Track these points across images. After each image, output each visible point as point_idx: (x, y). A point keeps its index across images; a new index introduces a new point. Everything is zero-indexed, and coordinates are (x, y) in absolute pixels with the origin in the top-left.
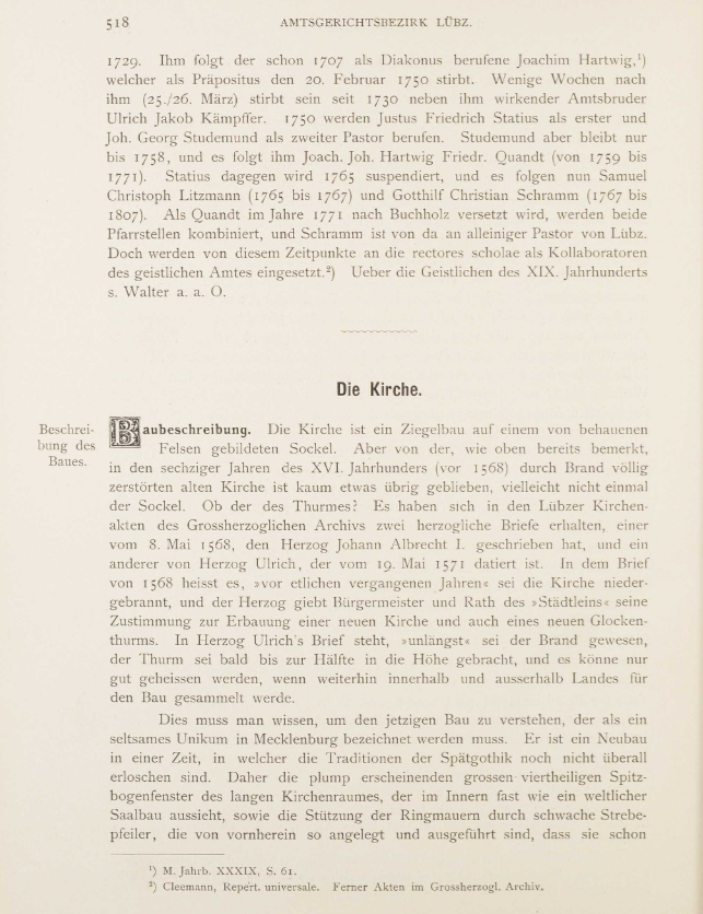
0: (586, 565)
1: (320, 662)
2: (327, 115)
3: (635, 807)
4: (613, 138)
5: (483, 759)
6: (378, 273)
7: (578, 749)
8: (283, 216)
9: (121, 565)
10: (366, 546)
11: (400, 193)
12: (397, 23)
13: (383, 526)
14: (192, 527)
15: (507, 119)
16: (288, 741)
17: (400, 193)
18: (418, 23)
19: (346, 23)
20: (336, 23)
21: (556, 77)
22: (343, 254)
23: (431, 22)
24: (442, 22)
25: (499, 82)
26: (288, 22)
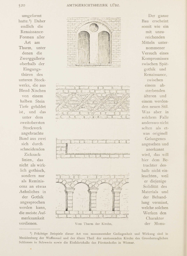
0: (36, 118)
2: (143, 154)
4: (133, 239)
5: (32, 171)
8: (40, 21)
9: (38, 32)
10: (40, 208)
11: (33, 196)
12: (99, 5)
13: (40, 139)
14: (143, 239)
17: (33, 196)
18: (105, 5)
19: (85, 5)
20: (82, 5)
21: (143, 111)
23: (109, 5)
24: (112, 5)
25: (144, 113)
26: (69, 5)
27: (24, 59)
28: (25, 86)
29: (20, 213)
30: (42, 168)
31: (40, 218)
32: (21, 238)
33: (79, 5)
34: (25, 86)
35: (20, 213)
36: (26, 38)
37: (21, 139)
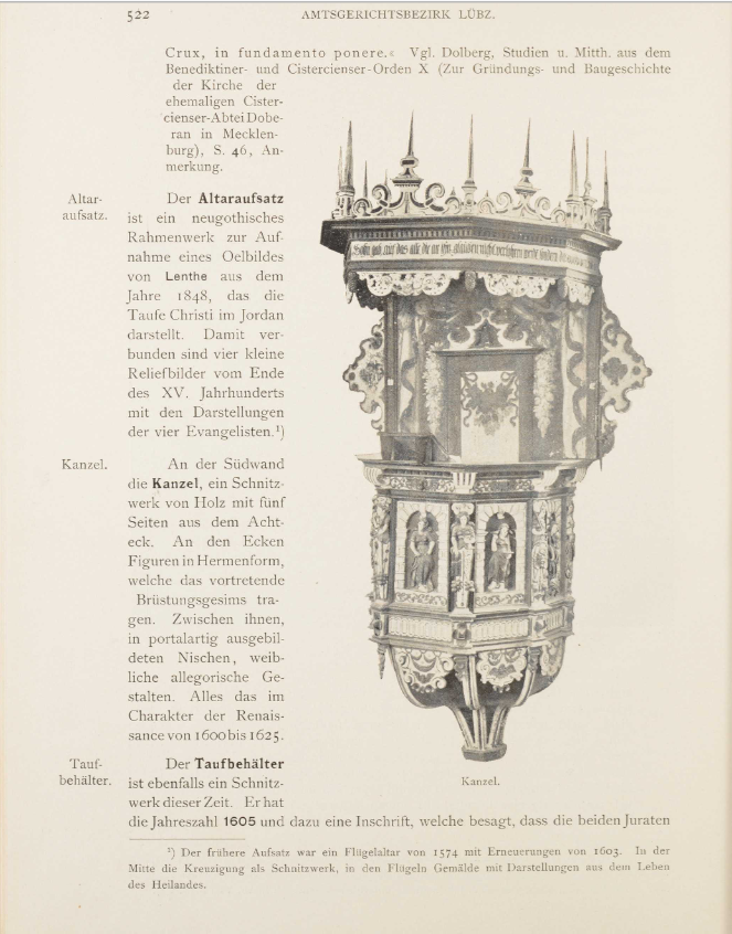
1: (200, 505)
3: (272, 111)
6: (659, 868)
7: (229, 345)
12: (420, 14)
14: (267, 679)
15: (139, 698)
16: (255, 135)
18: (441, 15)
22: (175, 717)
27: (187, 621)
28: (150, 505)
29: (132, 823)
30: (275, 569)
31: (268, 543)
32: (666, 70)
33: (346, 13)
34: (150, 505)
35: (132, 823)
36: (267, 562)
37: (589, 70)
